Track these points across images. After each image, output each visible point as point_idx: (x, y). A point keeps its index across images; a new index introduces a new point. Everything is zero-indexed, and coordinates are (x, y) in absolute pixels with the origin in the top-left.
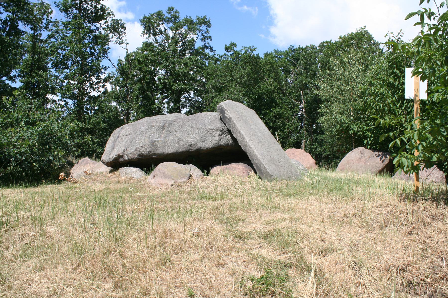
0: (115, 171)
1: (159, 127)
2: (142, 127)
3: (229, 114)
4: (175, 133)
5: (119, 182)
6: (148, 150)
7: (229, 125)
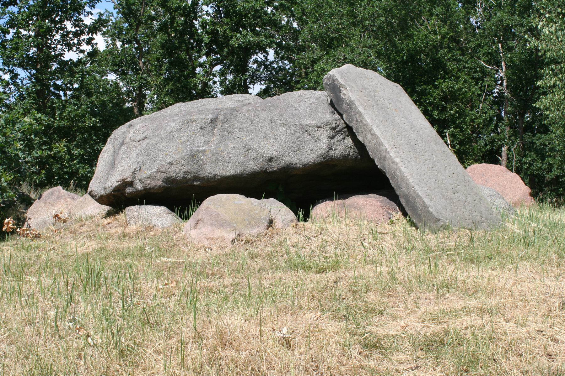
0: (117, 213)
1: (205, 123)
2: (171, 124)
3: (348, 94)
4: (238, 134)
5: (124, 236)
6: (184, 170)
7: (349, 116)
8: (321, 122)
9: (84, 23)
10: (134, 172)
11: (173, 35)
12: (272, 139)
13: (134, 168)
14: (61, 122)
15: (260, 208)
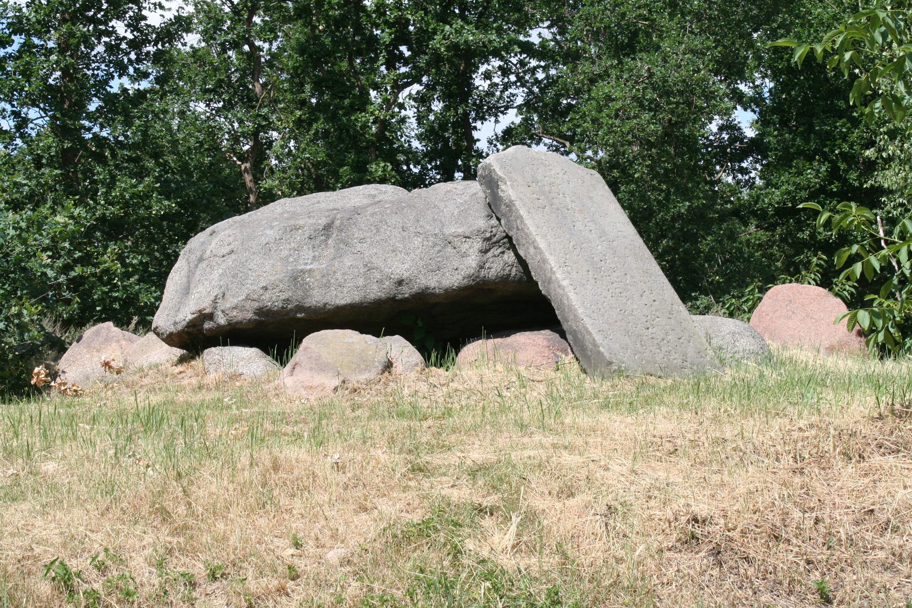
0: (193, 358)
1: (315, 231)
2: (268, 232)
3: (508, 191)
4: (359, 247)
5: (200, 388)
6: (283, 297)
7: (509, 221)
8: (471, 229)
9: (148, 22)
10: (215, 300)
11: (321, 27)
12: (403, 254)
13: (215, 294)
14: (107, 209)
15: (375, 347)
